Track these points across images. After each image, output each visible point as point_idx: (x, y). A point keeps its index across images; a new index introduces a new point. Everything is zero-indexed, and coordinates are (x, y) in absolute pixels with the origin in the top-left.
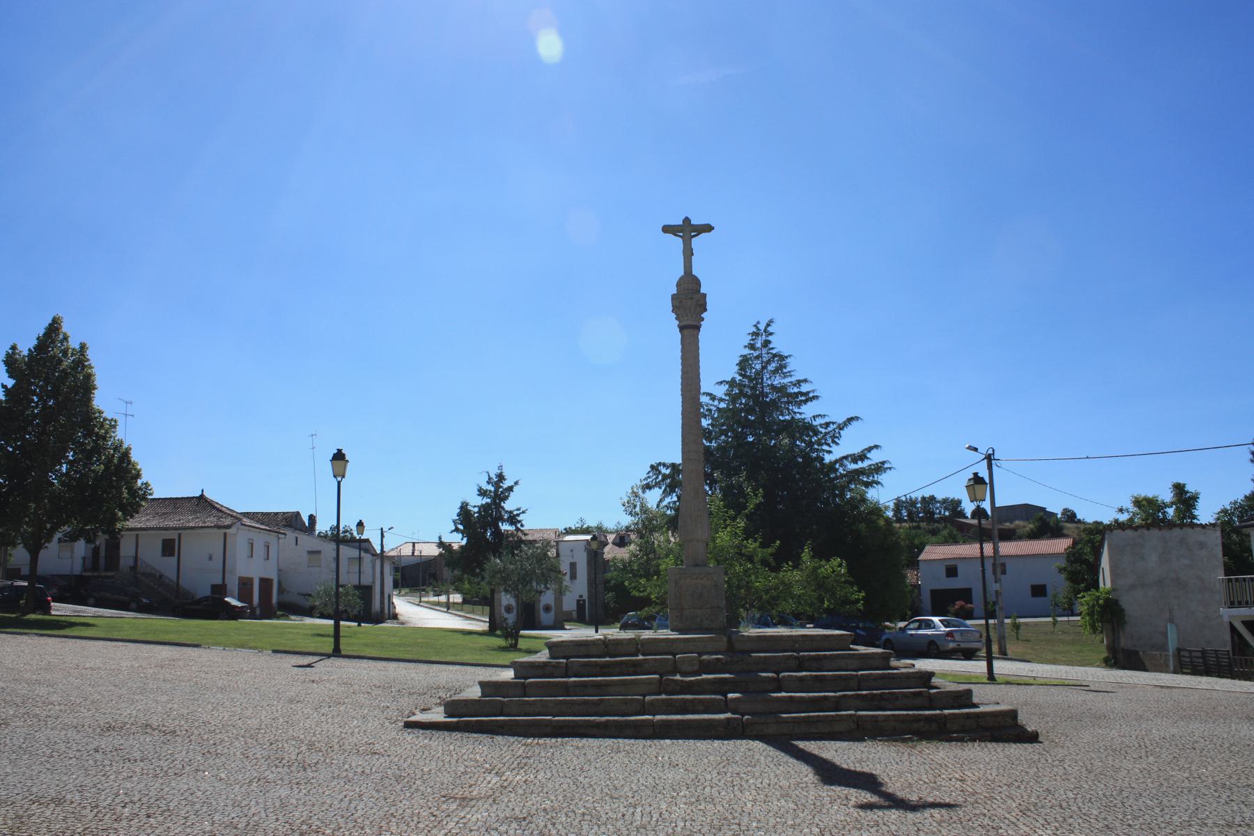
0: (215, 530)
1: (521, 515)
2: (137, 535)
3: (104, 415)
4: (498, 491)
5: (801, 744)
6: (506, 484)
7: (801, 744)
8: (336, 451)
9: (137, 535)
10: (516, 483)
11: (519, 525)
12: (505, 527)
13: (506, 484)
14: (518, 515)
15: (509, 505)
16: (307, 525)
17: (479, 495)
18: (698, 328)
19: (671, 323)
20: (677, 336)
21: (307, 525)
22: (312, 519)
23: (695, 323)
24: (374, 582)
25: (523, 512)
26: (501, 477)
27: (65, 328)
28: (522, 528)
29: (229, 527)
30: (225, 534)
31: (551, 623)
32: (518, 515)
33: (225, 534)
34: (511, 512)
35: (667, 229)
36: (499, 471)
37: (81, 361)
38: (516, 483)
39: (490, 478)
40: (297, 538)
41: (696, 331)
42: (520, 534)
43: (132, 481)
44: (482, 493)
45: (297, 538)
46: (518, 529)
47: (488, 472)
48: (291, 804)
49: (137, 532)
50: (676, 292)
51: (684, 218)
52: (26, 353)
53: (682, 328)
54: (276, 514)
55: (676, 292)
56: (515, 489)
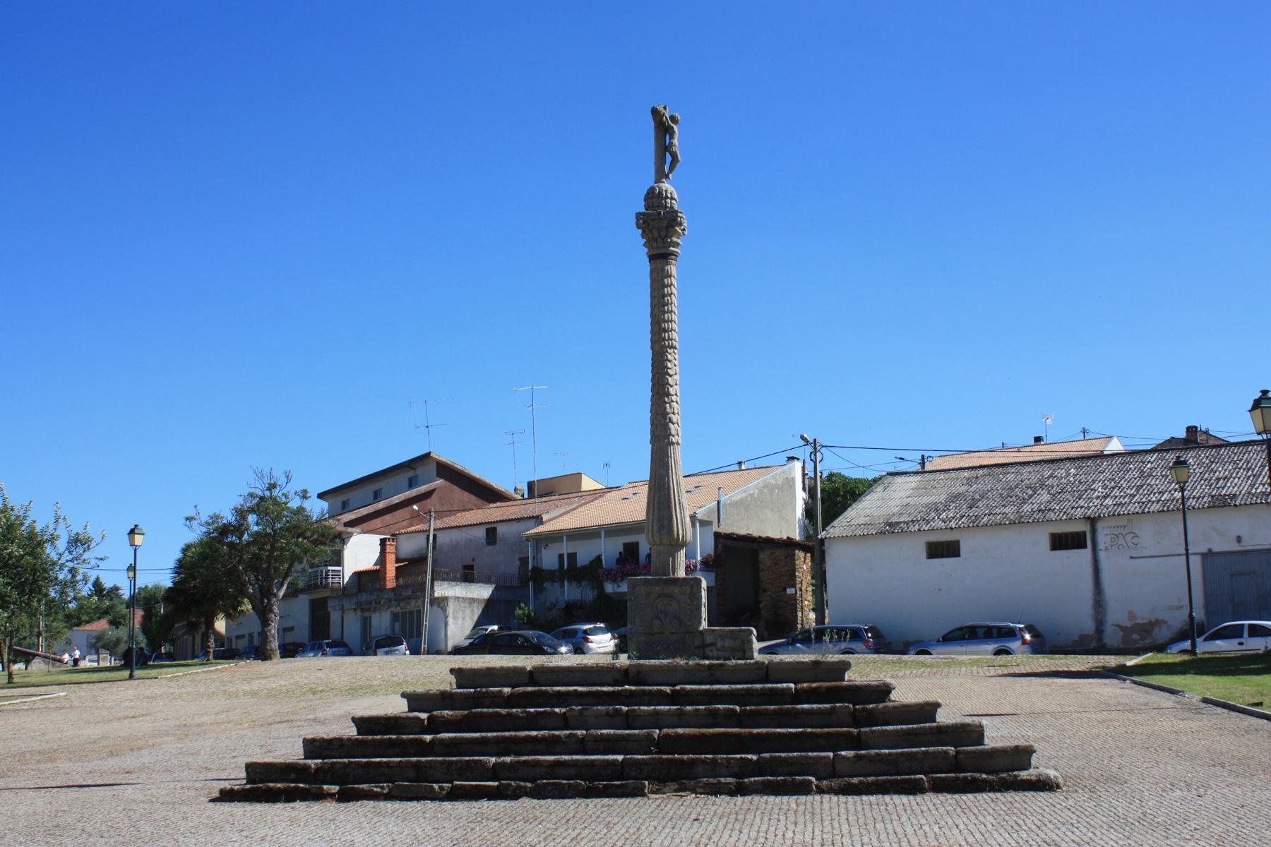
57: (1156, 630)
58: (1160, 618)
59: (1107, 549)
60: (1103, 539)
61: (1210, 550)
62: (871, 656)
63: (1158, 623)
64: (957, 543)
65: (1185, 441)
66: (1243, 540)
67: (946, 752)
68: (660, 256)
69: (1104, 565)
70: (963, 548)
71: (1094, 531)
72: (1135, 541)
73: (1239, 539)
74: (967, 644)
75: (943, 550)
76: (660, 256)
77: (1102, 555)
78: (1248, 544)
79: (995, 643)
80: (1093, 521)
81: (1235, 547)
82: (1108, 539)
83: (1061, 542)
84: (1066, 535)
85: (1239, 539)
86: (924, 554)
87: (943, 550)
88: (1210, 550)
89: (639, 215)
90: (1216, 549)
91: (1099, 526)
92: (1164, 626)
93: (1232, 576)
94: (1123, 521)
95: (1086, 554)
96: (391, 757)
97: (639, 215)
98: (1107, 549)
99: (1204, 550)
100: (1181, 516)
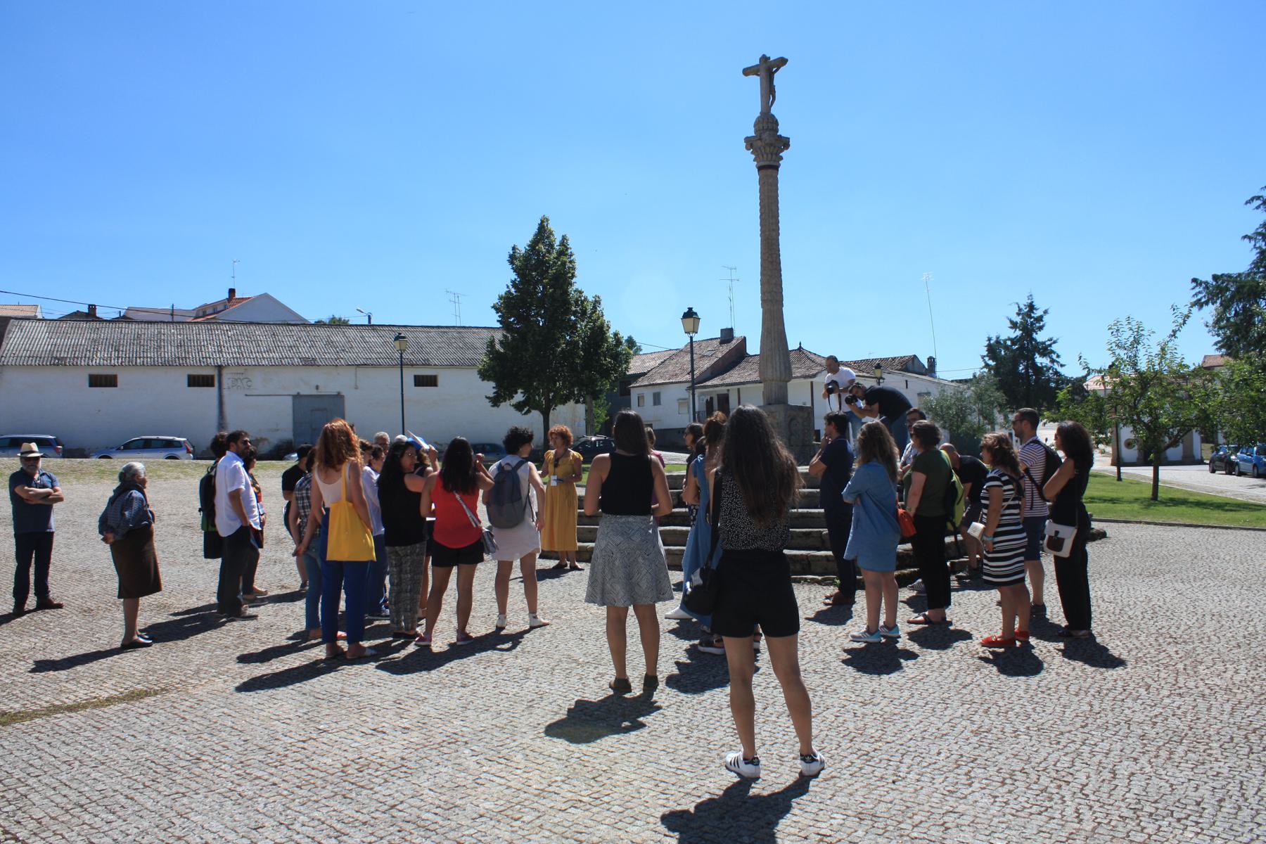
0: (802, 380)
1: (1053, 345)
2: (739, 390)
3: (583, 294)
4: (1029, 321)
5: (499, 647)
6: (1037, 313)
7: (499, 647)
8: (686, 310)
9: (739, 390)
10: (1046, 312)
11: (1054, 356)
12: (1040, 360)
13: (1037, 313)
14: (1050, 345)
15: (1040, 337)
16: (927, 367)
17: (1011, 328)
18: (776, 168)
19: (748, 162)
20: (755, 176)
21: (927, 367)
22: (932, 361)
23: (772, 163)
24: (206, 465)
25: (1055, 342)
26: (1031, 307)
27: (552, 226)
28: (1057, 359)
29: (814, 376)
30: (812, 383)
31: (1134, 460)
32: (1050, 345)
33: (812, 383)
34: (1044, 343)
35: (747, 72)
36: (1029, 301)
37: (564, 250)
38: (1046, 312)
39: (1020, 310)
40: (907, 381)
41: (775, 171)
42: (1056, 366)
43: (1237, 307)
44: (1014, 325)
45: (907, 381)
46: (1053, 361)
47: (1017, 304)
48: (1164, 651)
49: (739, 387)
50: (753, 134)
51: (786, 57)
52: (523, 251)
53: (760, 168)
54: (894, 359)
55: (753, 134)
56: (1046, 318)
57: (261, 445)
58: (264, 437)
59: (229, 388)
60: (227, 381)
61: (298, 393)
62: (59, 459)
63: (262, 440)
64: (115, 377)
65: (87, 315)
66: (320, 388)
67: (821, 532)
68: (769, 168)
69: (226, 399)
70: (120, 380)
71: (220, 375)
72: (249, 384)
73: (317, 387)
74: (144, 452)
75: (102, 381)
76: (769, 168)
77: (225, 392)
78: (323, 391)
79: (166, 451)
80: (220, 368)
81: (314, 392)
82: (230, 382)
83: (195, 381)
84: (101, 376)
85: (317, 387)
86: (87, 384)
87: (102, 381)
88: (298, 393)
89: (748, 140)
90: (302, 393)
91: (225, 372)
92: (266, 442)
93: (312, 410)
94: (241, 370)
95: (212, 392)
96: (810, 550)
97: (748, 140)
98: (229, 388)
99: (295, 393)
100: (399, 369)
